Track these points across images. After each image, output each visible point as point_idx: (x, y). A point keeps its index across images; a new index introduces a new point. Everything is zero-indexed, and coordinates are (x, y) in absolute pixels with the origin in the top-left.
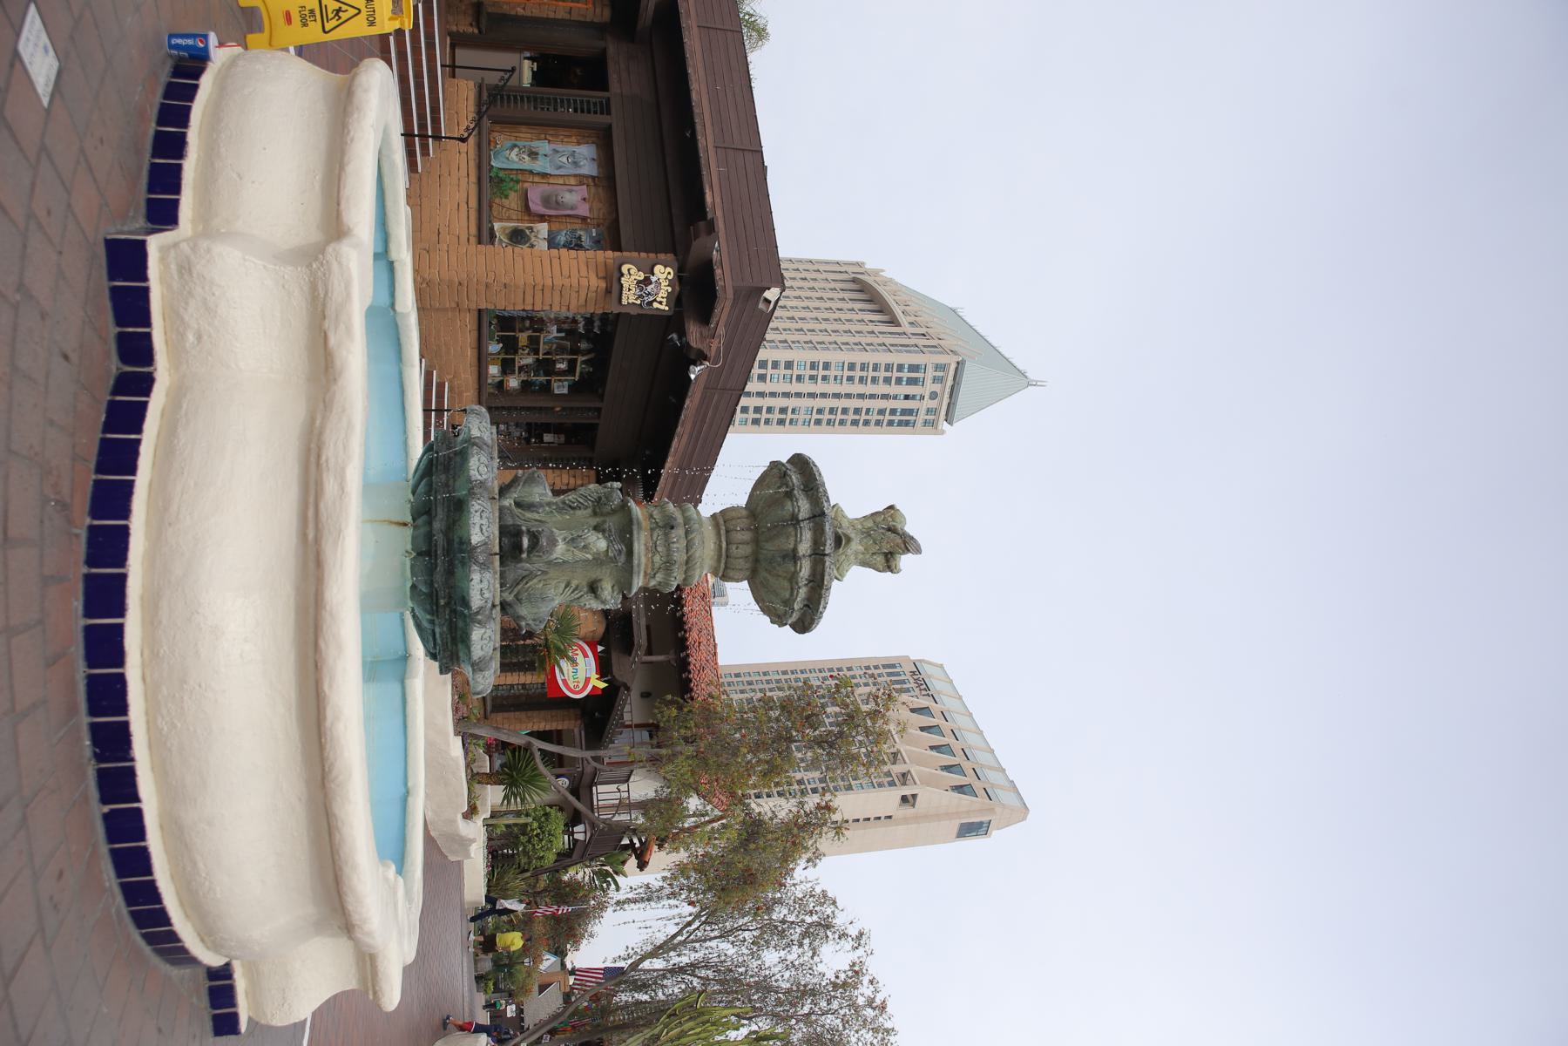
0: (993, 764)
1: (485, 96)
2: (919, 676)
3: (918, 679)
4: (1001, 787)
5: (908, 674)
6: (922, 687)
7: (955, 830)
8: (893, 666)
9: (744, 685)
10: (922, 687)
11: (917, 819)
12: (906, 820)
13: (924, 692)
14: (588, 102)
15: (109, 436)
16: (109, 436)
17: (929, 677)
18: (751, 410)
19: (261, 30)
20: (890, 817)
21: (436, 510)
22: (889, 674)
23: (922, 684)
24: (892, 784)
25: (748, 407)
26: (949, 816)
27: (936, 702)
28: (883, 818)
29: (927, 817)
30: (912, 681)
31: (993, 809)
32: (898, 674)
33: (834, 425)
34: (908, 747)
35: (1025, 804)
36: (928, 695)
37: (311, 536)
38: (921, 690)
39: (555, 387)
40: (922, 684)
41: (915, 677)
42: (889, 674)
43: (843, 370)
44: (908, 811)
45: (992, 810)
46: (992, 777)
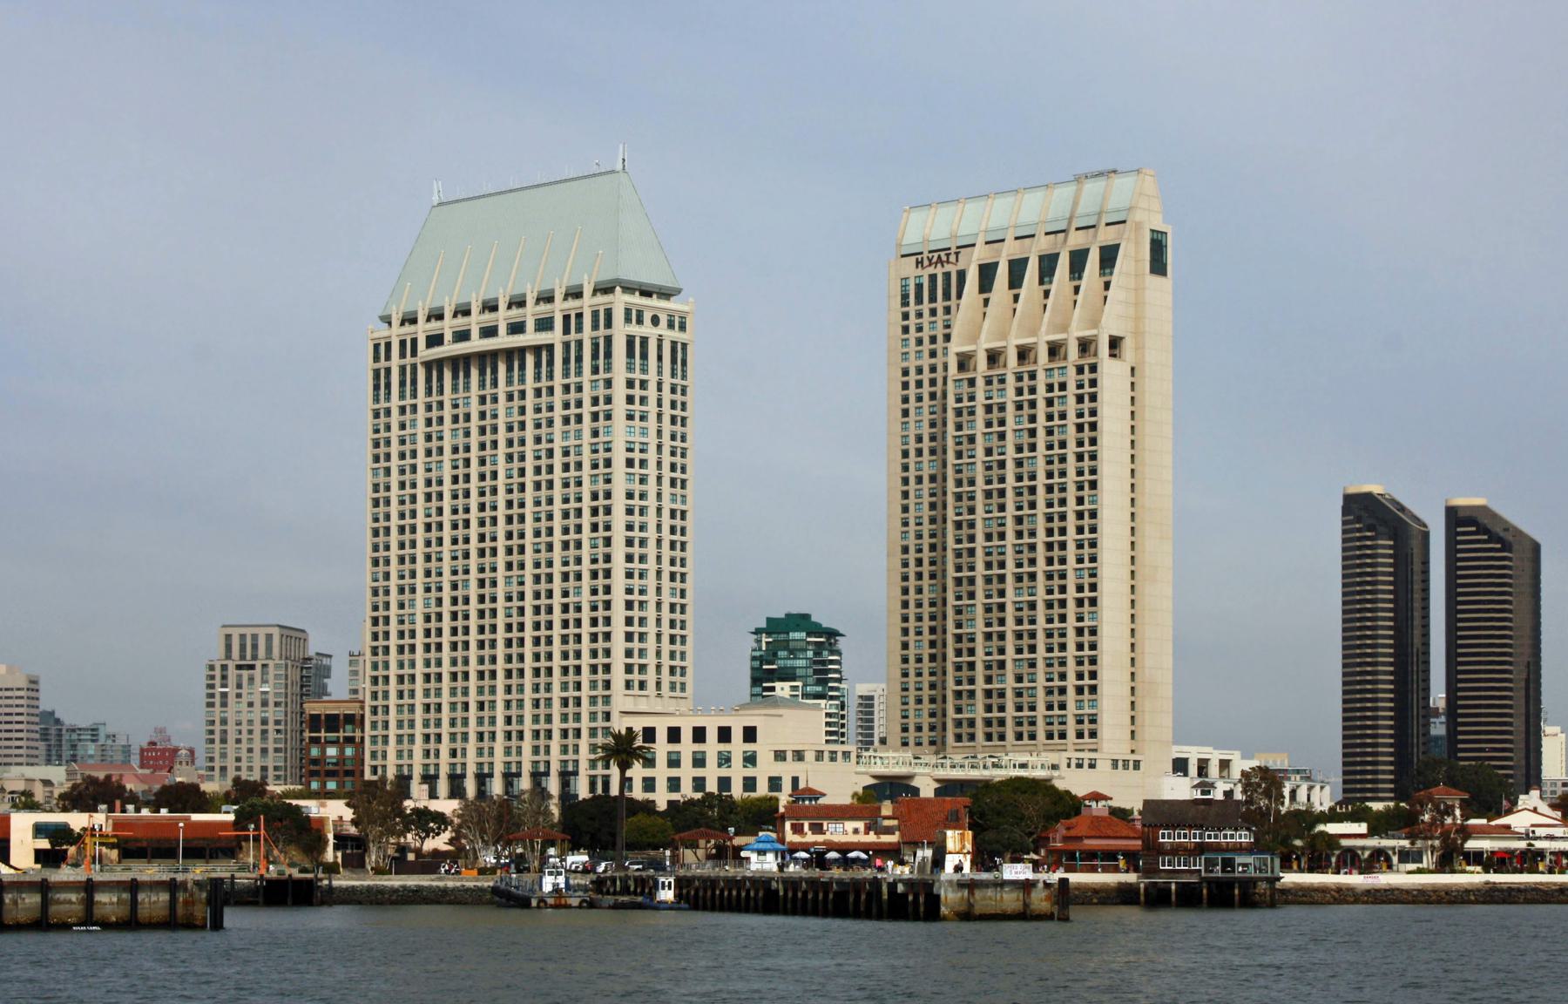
3: (930, 260)
5: (919, 272)
9: (921, 421)
10: (944, 258)
11: (1138, 334)
12: (1139, 348)
13: (952, 258)
14: (255, 637)
20: (1133, 369)
21: (760, 715)
23: (939, 257)
24: (1093, 368)
26: (1139, 290)
28: (1133, 539)
29: (1138, 319)
30: (931, 270)
32: (919, 287)
33: (647, 444)
34: (1043, 329)
36: (957, 254)
37: (1381, 795)
38: (948, 262)
40: (939, 257)
41: (926, 263)
42: (919, 300)
43: (634, 474)
44: (1128, 347)
45: (1138, 226)
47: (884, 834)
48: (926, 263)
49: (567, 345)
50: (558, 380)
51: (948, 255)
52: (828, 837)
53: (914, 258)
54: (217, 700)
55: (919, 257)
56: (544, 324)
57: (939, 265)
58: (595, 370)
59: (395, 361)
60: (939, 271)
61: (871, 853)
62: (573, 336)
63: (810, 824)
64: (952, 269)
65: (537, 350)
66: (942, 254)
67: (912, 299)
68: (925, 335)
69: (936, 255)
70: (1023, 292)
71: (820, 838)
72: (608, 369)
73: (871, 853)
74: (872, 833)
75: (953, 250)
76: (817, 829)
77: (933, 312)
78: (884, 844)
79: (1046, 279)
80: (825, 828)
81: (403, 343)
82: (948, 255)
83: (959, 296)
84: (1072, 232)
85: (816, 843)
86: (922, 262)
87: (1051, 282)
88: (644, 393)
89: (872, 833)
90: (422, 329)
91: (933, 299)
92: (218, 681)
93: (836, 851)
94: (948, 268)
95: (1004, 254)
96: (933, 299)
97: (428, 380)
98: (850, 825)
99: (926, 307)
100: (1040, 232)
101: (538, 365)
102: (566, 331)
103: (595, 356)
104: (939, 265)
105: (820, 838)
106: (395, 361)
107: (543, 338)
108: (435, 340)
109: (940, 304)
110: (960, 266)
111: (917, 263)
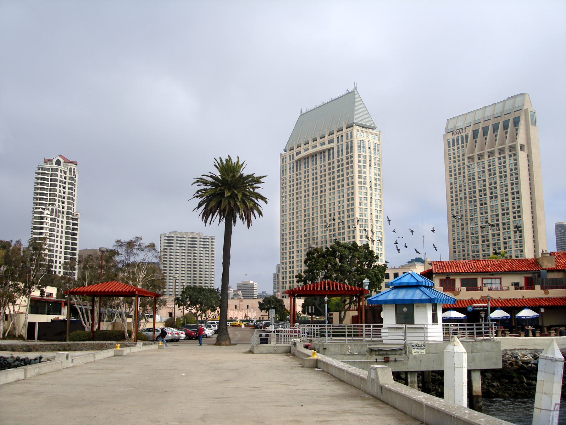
0: (502, 104)
1: (477, 387)
2: (455, 132)
3: (457, 132)
4: (504, 107)
5: (453, 137)
6: (461, 131)
7: (534, 127)
8: (449, 143)
10: (461, 131)
13: (464, 131)
15: (46, 312)
16: (46, 312)
17: (455, 127)
18: (360, 159)
19: (398, 322)
22: (453, 145)
23: (459, 131)
24: (515, 155)
25: (358, 160)
27: (480, 122)
30: (457, 135)
31: (525, 110)
35: (512, 97)
36: (465, 129)
38: (462, 132)
39: (344, 242)
40: (459, 131)
41: (455, 133)
46: (508, 106)
47: (552, 288)
48: (455, 133)
49: (338, 146)
50: (336, 158)
51: (462, 130)
52: (486, 292)
53: (451, 133)
54: (276, 283)
55: (453, 132)
56: (331, 141)
57: (460, 133)
58: (347, 153)
59: (288, 162)
60: (460, 135)
61: (542, 310)
62: (340, 143)
63: (462, 280)
64: (464, 134)
65: (329, 150)
66: (460, 130)
67: (451, 145)
68: (456, 155)
69: (458, 131)
70: (488, 136)
71: (475, 295)
72: (352, 151)
73: (542, 310)
74: (538, 287)
75: (464, 128)
76: (471, 285)
77: (458, 148)
78: (555, 299)
79: (496, 131)
80: (479, 284)
81: (290, 156)
82: (462, 130)
83: (467, 142)
84: (503, 116)
85: (472, 301)
86: (454, 134)
87: (497, 132)
88: (364, 159)
89: (538, 287)
90: (296, 150)
91: (458, 144)
92: (276, 278)
93: (529, 308)
94: (462, 134)
95: (481, 126)
96: (458, 144)
97: (297, 166)
98: (508, 281)
99: (456, 147)
100: (492, 118)
101: (329, 155)
102: (338, 142)
103: (347, 148)
104: (460, 133)
105: (475, 295)
106: (288, 162)
107: (331, 145)
108: (298, 153)
109: (460, 145)
110: (466, 133)
111: (452, 134)
